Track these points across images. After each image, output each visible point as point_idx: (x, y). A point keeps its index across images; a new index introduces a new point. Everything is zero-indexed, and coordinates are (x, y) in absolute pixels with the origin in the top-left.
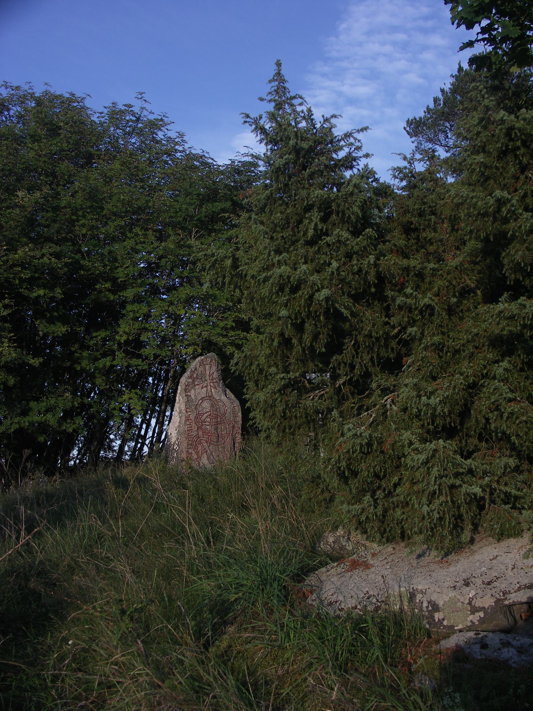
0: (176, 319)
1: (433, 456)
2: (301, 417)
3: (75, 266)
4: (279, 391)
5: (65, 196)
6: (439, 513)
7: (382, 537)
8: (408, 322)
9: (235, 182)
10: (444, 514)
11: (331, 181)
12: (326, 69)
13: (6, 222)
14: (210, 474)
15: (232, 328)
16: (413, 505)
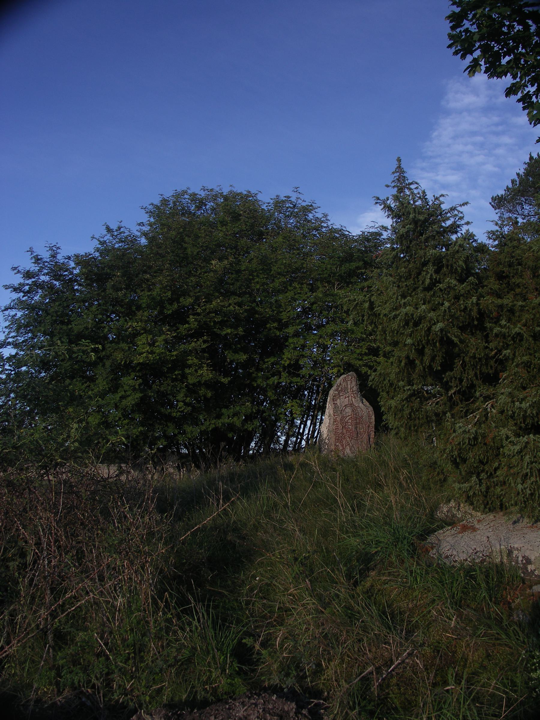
0: (325, 348)
1: (526, 447)
2: (422, 418)
3: (252, 312)
4: (406, 399)
5: (244, 262)
6: (530, 490)
7: (485, 508)
8: (503, 346)
9: (365, 247)
10: (534, 491)
11: (441, 243)
12: (424, 164)
13: (204, 283)
14: (353, 461)
15: (366, 354)
16: (510, 484)
